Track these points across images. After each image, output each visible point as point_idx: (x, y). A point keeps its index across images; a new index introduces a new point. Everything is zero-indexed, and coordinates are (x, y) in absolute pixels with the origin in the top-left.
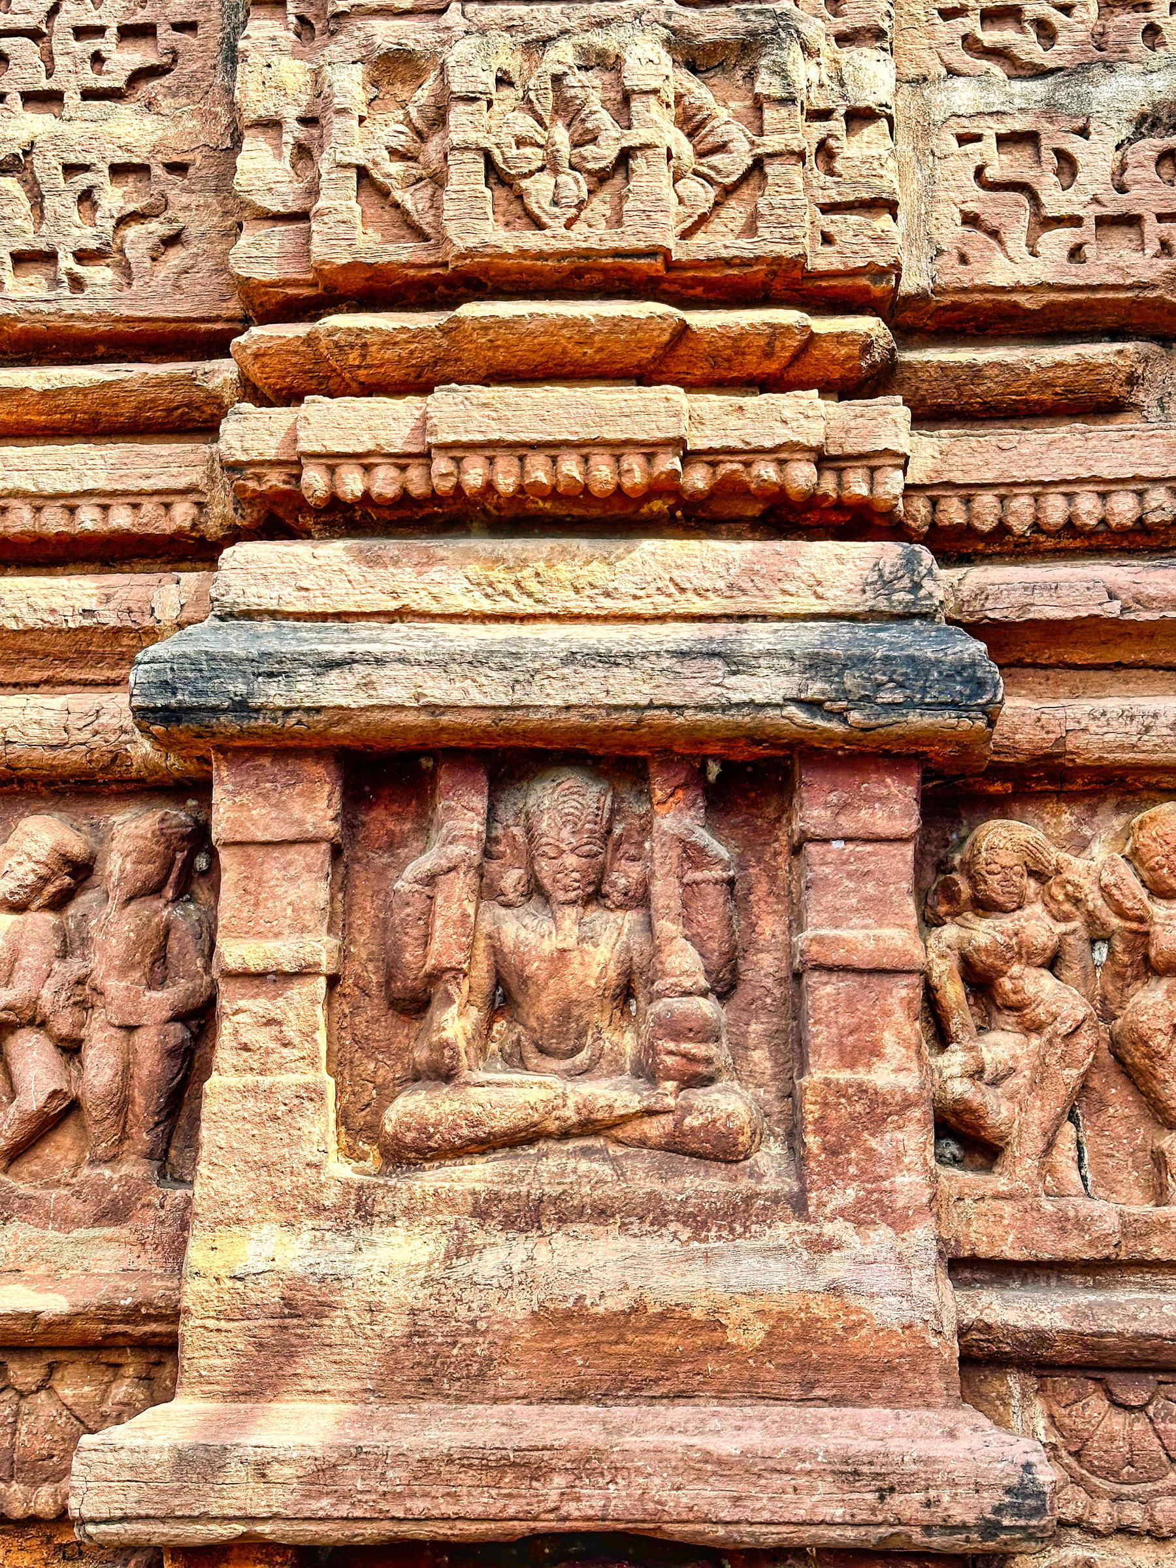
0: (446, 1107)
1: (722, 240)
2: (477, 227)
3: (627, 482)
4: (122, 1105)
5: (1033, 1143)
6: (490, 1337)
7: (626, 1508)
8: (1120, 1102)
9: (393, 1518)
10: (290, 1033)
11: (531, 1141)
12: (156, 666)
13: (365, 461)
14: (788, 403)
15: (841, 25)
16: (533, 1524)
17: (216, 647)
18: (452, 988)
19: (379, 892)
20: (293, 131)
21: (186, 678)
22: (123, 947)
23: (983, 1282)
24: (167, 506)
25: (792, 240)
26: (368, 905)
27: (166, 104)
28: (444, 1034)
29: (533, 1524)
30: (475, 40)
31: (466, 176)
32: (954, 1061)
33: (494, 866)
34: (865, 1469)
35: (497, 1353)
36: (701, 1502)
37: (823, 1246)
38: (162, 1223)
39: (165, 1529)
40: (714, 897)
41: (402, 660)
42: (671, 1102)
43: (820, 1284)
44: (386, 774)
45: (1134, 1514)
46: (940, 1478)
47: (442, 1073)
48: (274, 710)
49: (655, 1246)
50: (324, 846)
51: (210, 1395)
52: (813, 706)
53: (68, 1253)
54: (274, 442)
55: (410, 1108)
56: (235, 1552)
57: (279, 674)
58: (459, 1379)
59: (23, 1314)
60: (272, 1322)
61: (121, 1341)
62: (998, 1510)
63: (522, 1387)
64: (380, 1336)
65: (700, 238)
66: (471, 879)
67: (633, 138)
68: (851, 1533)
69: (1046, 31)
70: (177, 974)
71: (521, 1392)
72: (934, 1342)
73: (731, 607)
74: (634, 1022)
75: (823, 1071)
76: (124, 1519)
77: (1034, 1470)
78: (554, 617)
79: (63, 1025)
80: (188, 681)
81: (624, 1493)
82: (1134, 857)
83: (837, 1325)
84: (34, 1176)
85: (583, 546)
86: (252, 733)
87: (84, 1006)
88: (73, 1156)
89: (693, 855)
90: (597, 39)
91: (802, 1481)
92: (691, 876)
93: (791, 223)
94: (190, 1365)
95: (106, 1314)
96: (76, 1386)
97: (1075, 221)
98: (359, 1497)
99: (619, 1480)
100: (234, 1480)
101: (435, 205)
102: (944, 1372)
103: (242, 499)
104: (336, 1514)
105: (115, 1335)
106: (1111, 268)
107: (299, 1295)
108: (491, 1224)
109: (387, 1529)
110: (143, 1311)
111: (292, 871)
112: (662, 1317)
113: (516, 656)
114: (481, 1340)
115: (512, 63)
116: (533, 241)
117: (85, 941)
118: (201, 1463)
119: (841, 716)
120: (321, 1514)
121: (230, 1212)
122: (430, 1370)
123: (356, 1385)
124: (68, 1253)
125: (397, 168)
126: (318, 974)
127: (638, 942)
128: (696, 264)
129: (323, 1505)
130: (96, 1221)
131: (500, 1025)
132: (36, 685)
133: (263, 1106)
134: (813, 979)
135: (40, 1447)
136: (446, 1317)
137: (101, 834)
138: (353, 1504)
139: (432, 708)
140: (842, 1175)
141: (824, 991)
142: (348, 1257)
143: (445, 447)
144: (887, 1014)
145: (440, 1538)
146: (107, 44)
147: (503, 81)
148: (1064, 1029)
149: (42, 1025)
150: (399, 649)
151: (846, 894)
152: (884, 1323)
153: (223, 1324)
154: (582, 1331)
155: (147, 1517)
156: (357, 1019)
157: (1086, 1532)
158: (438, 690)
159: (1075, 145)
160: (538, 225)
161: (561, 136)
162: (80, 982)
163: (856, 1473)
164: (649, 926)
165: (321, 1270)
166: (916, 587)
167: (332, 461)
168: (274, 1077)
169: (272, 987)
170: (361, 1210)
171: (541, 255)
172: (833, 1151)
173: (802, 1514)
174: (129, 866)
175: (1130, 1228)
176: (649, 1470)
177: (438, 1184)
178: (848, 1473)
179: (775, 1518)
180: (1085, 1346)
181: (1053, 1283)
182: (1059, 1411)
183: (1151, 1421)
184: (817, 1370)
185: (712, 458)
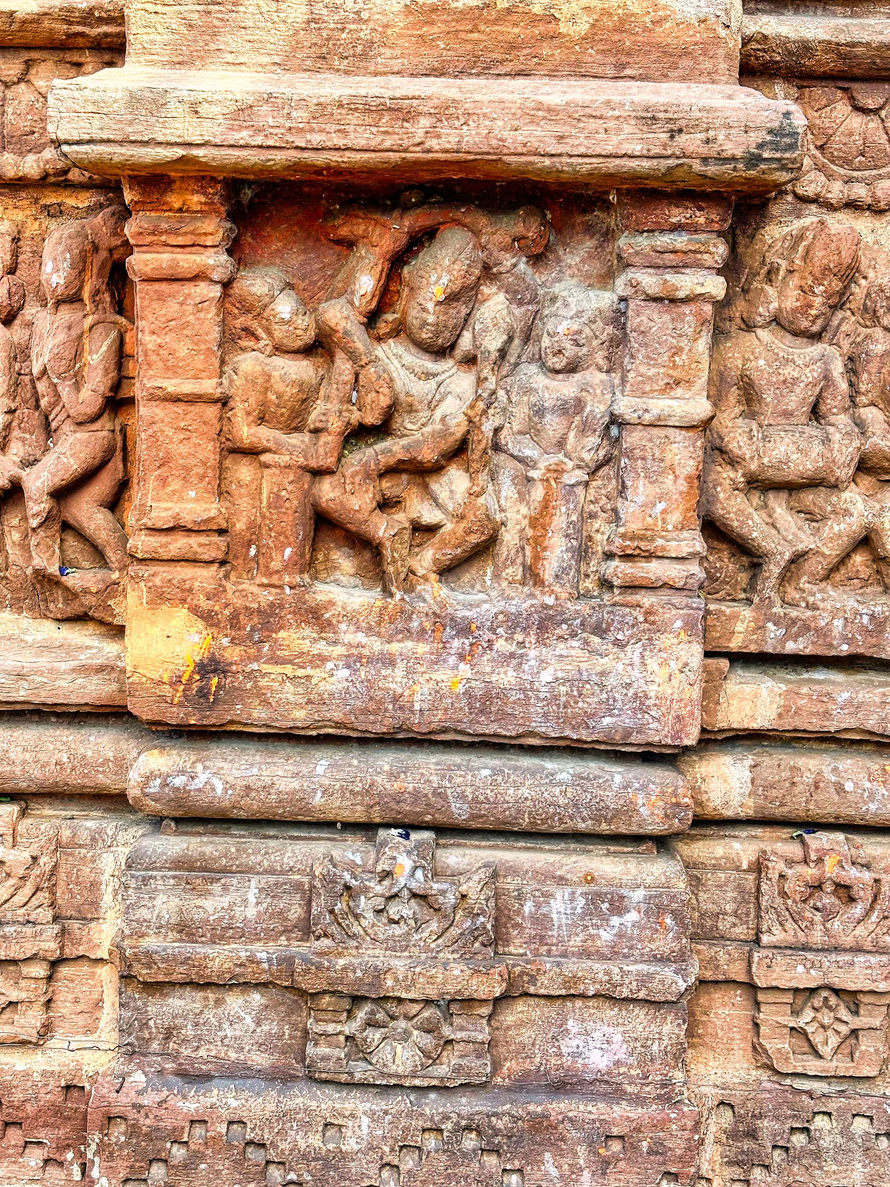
6: (371, 25)
7: (475, 144)
9: (297, 148)
16: (403, 155)
23: (764, 12)
29: (403, 155)
34: (661, 115)
35: (376, 37)
36: (533, 139)
39: (123, 150)
45: (860, 191)
46: (718, 122)
51: (153, 63)
56: (178, 184)
58: (347, 58)
61: (80, 41)
62: (760, 146)
63: (396, 65)
68: (646, 164)
71: (396, 69)
72: (723, 33)
76: (90, 142)
77: (791, 117)
81: (473, 132)
83: (647, 19)
91: (611, 124)
94: (135, 39)
95: (67, 16)
98: (271, 130)
99: (471, 123)
100: (175, 114)
102: (728, 57)
104: (253, 143)
110: (97, 14)
114: (364, 27)
120: (242, 142)
122: (324, 50)
123: (266, 59)
129: (243, 136)
138: (266, 136)
145: (333, 164)
152: (684, 17)
153: (159, 8)
154: (445, 21)
155: (109, 141)
157: (821, 206)
163: (654, 118)
173: (609, 149)
176: (495, 116)
178: (648, 119)
179: (590, 152)
180: (840, 55)
181: (819, 12)
183: (883, 121)
184: (629, 54)
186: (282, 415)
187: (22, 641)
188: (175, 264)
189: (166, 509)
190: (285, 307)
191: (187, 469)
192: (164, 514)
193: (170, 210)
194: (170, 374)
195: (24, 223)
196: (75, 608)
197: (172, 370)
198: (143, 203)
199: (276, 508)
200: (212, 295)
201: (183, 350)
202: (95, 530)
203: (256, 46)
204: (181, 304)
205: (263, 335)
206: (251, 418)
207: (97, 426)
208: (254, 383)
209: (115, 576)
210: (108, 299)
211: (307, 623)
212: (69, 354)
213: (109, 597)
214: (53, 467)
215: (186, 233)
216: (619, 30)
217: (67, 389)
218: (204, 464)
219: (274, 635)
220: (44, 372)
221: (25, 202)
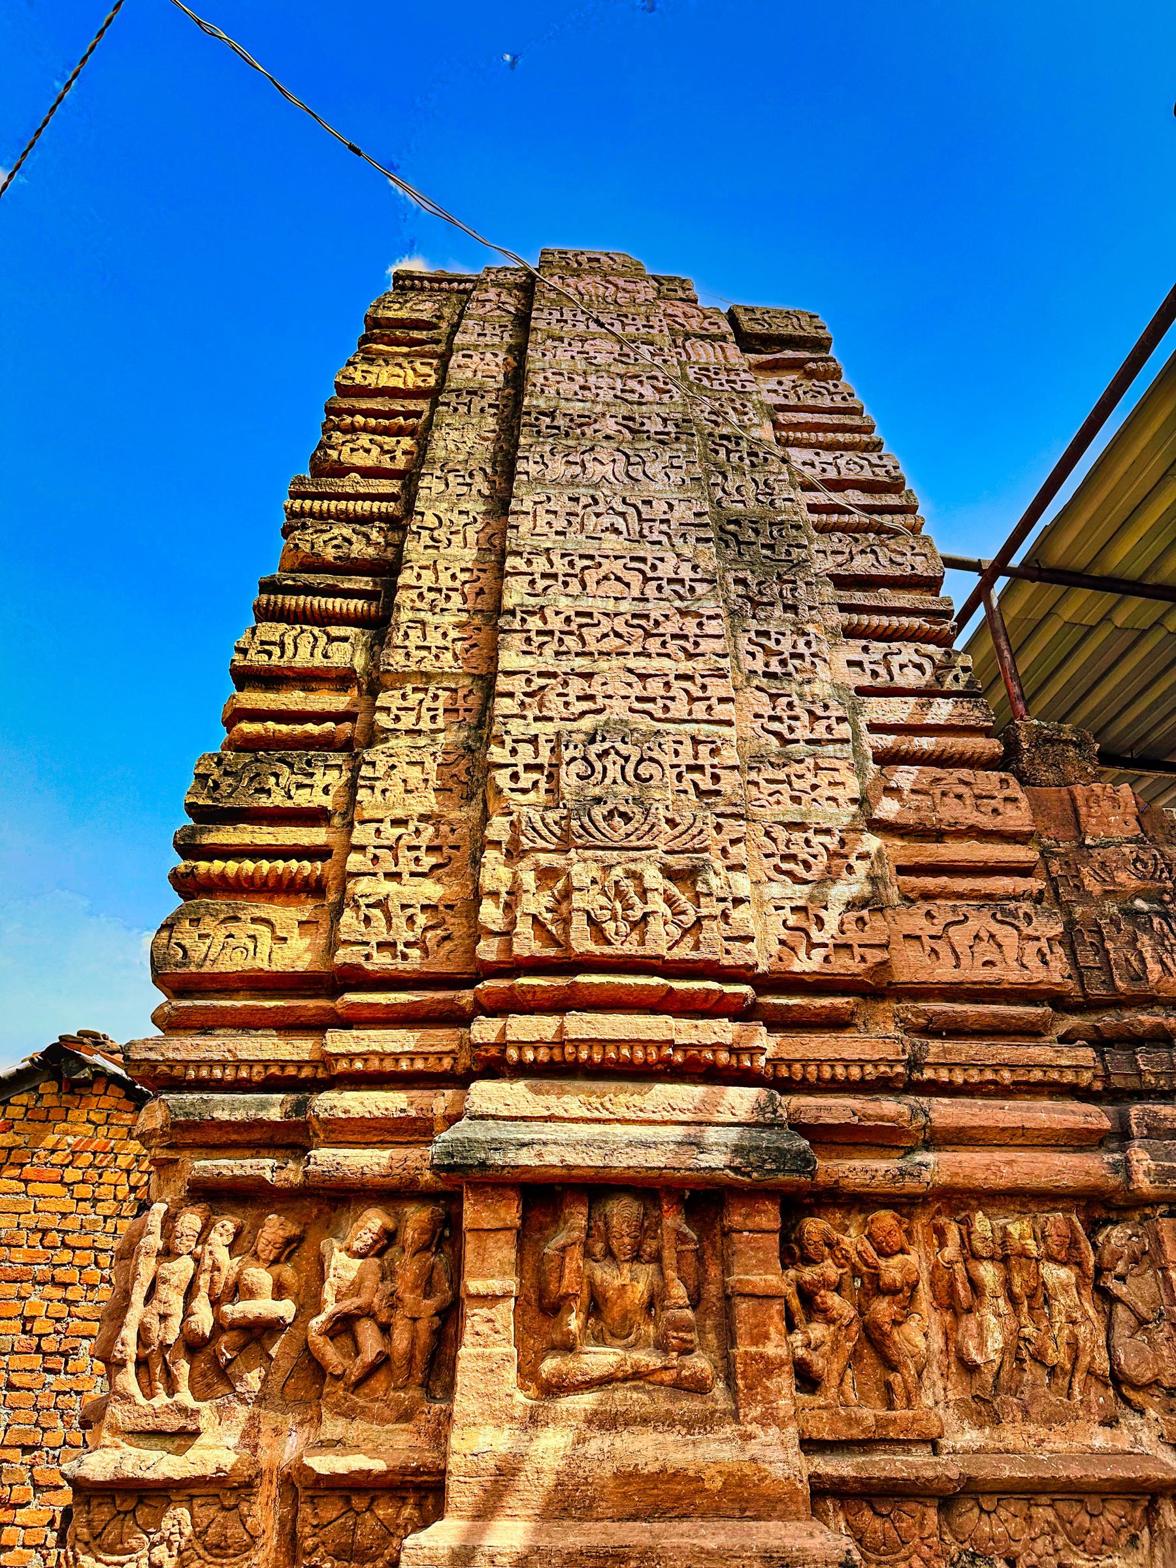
1: (684, 952)
2: (582, 943)
3: (650, 1059)
4: (411, 1359)
5: (835, 1381)
8: (869, 1358)
10: (498, 1326)
11: (609, 1383)
13: (535, 1045)
14: (715, 1024)
15: (728, 862)
17: (471, 1135)
20: (504, 897)
24: (440, 1059)
25: (715, 953)
27: (445, 879)
30: (582, 864)
31: (579, 921)
32: (797, 1338)
33: (590, 1241)
37: (748, 1437)
40: (691, 1258)
42: (675, 1362)
43: (747, 1457)
44: (545, 1196)
46: (809, 1559)
47: (567, 1347)
49: (670, 1438)
51: (461, 1517)
52: (736, 1170)
54: (494, 1035)
63: (610, 1512)
65: (675, 950)
66: (582, 1249)
67: (648, 909)
69: (807, 866)
73: (697, 1118)
74: (654, 1320)
75: (743, 1347)
78: (618, 1121)
79: (383, 1318)
82: (870, 1236)
84: (366, 1395)
85: (630, 1086)
87: (392, 1307)
89: (682, 1238)
90: (632, 866)
92: (680, 1248)
93: (714, 945)
95: (404, 1470)
97: (825, 945)
101: (566, 933)
103: (476, 1059)
106: (842, 967)
108: (593, 1427)
112: (674, 1475)
113: (606, 1142)
115: (598, 875)
116: (607, 950)
117: (393, 1273)
119: (748, 1175)
121: (471, 1420)
123: (531, 1512)
125: (549, 916)
127: (656, 1280)
128: (674, 961)
131: (592, 1321)
133: (486, 1364)
134: (738, 1300)
135: (367, 1542)
136: (574, 1476)
137: (399, 1218)
139: (568, 1167)
140: (755, 1400)
141: (743, 1307)
143: (571, 1041)
144: (771, 1318)
146: (421, 854)
147: (594, 882)
148: (845, 1322)
151: (750, 1258)
158: (573, 1159)
159: (823, 913)
160: (609, 943)
161: (618, 906)
162: (392, 1294)
164: (661, 1272)
165: (514, 1451)
166: (775, 1111)
167: (520, 1045)
168: (488, 1346)
170: (533, 1421)
171: (611, 956)
172: (750, 1388)
175: (881, 1423)
182: (851, 1518)
185: (684, 1048)
216: (740, 1485)
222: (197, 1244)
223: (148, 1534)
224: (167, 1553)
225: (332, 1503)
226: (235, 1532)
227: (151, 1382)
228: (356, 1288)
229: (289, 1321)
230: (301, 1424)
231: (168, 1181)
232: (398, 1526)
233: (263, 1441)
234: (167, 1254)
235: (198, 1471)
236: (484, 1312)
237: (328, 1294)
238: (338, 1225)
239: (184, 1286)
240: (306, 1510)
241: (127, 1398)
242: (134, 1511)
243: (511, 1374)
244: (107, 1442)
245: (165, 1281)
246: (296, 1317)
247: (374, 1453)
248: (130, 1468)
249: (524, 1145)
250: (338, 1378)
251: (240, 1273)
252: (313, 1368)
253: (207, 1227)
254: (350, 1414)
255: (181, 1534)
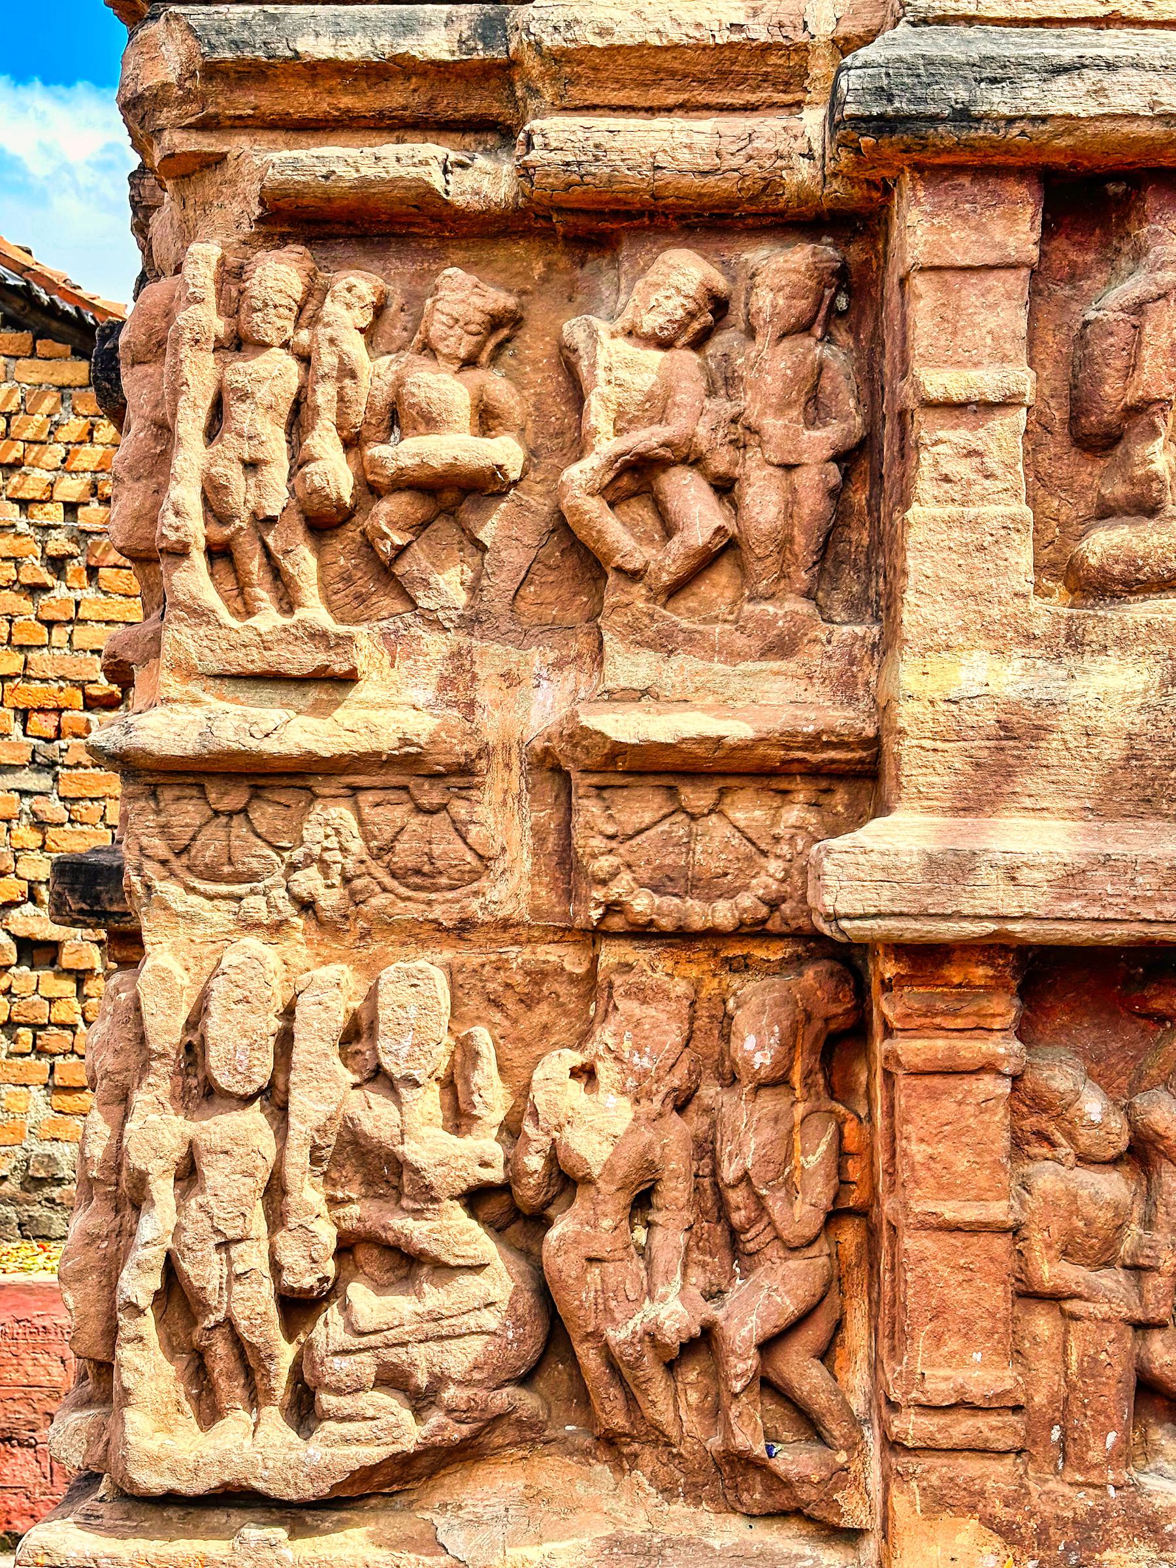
0: (1155, 540)
9: (1144, 920)
10: (992, 464)
12: (870, 71)
18: (1159, 421)
19: (1061, 326)
21: (903, 84)
22: (779, 385)
26: (1050, 339)
28: (1153, 467)
38: (830, 657)
39: (917, 925)
41: (1135, 66)
48: (996, 120)
50: (1025, 272)
51: (930, 810)
53: (736, 684)
55: (1104, 544)
56: (957, 954)
57: (1003, 80)
59: (708, 738)
60: (988, 744)
64: (1097, 759)
70: (828, 415)
76: (878, 915)
80: (905, 88)
84: (692, 611)
86: (969, 146)
88: (729, 594)
95: (788, 740)
96: (745, 809)
100: (985, 882)
104: (1087, 916)
105: (793, 761)
107: (1015, 719)
109: (1136, 930)
111: (991, 298)
118: (954, 867)
120: (1072, 914)
122: (1149, 791)
123: (1074, 804)
124: (736, 684)
126: (1021, 404)
129: (1074, 907)
130: (762, 655)
132: (669, 110)
133: (970, 537)
135: (716, 866)
138: (1103, 906)
142: (1063, 684)
149: (695, 461)
150: (1132, 53)
153: (939, 745)
155: (901, 914)
156: (1040, 457)
162: (734, 421)
165: (1037, 695)
168: (967, 510)
169: (973, 418)
174: (781, 302)
177: (1149, 616)
186: (1092, 1247)
187: (706, 1547)
188: (953, 1052)
189: (946, 1379)
190: (1093, 1105)
191: (968, 1322)
192: (943, 1386)
193: (946, 985)
194: (943, 1195)
195: (699, 980)
196: (782, 1500)
197: (946, 1189)
198: (912, 977)
199: (1093, 1376)
200: (999, 1091)
201: (962, 1163)
202: (809, 1392)
203: (1063, 788)
204: (960, 1103)
205: (1063, 1141)
206: (1053, 1253)
207: (814, 1251)
208: (1056, 1205)
209: (842, 1457)
210: (822, 1081)
211: (1142, 1537)
212: (779, 1156)
213: (835, 1489)
214: (762, 1308)
215: (968, 1015)
217: (779, 1203)
218: (992, 1315)
219: (1097, 1556)
220: (745, 1178)
221: (703, 955)
222: (297, 326)
223: (279, 849)
224: (319, 881)
225: (641, 799)
226: (448, 848)
227: (242, 587)
228: (657, 406)
229: (514, 475)
230: (558, 665)
231: (206, 205)
232: (777, 839)
233: (485, 695)
234: (239, 343)
235: (363, 744)
236: (960, 435)
237: (598, 415)
238: (593, 293)
239: (285, 408)
240: (589, 809)
241: (199, 614)
242: (244, 811)
243: (1022, 556)
244: (173, 694)
245: (244, 396)
246: (525, 472)
247: (724, 706)
248: (230, 734)
249: (1060, 70)
250: (634, 576)
251: (399, 383)
252: (578, 557)
253: (315, 293)
254: (664, 644)
255: (343, 850)
